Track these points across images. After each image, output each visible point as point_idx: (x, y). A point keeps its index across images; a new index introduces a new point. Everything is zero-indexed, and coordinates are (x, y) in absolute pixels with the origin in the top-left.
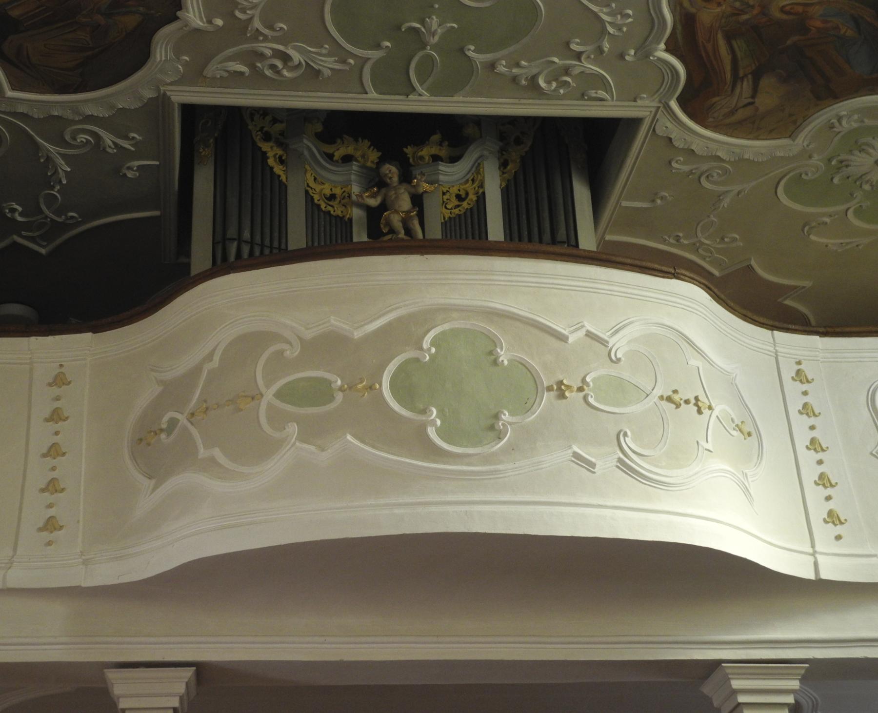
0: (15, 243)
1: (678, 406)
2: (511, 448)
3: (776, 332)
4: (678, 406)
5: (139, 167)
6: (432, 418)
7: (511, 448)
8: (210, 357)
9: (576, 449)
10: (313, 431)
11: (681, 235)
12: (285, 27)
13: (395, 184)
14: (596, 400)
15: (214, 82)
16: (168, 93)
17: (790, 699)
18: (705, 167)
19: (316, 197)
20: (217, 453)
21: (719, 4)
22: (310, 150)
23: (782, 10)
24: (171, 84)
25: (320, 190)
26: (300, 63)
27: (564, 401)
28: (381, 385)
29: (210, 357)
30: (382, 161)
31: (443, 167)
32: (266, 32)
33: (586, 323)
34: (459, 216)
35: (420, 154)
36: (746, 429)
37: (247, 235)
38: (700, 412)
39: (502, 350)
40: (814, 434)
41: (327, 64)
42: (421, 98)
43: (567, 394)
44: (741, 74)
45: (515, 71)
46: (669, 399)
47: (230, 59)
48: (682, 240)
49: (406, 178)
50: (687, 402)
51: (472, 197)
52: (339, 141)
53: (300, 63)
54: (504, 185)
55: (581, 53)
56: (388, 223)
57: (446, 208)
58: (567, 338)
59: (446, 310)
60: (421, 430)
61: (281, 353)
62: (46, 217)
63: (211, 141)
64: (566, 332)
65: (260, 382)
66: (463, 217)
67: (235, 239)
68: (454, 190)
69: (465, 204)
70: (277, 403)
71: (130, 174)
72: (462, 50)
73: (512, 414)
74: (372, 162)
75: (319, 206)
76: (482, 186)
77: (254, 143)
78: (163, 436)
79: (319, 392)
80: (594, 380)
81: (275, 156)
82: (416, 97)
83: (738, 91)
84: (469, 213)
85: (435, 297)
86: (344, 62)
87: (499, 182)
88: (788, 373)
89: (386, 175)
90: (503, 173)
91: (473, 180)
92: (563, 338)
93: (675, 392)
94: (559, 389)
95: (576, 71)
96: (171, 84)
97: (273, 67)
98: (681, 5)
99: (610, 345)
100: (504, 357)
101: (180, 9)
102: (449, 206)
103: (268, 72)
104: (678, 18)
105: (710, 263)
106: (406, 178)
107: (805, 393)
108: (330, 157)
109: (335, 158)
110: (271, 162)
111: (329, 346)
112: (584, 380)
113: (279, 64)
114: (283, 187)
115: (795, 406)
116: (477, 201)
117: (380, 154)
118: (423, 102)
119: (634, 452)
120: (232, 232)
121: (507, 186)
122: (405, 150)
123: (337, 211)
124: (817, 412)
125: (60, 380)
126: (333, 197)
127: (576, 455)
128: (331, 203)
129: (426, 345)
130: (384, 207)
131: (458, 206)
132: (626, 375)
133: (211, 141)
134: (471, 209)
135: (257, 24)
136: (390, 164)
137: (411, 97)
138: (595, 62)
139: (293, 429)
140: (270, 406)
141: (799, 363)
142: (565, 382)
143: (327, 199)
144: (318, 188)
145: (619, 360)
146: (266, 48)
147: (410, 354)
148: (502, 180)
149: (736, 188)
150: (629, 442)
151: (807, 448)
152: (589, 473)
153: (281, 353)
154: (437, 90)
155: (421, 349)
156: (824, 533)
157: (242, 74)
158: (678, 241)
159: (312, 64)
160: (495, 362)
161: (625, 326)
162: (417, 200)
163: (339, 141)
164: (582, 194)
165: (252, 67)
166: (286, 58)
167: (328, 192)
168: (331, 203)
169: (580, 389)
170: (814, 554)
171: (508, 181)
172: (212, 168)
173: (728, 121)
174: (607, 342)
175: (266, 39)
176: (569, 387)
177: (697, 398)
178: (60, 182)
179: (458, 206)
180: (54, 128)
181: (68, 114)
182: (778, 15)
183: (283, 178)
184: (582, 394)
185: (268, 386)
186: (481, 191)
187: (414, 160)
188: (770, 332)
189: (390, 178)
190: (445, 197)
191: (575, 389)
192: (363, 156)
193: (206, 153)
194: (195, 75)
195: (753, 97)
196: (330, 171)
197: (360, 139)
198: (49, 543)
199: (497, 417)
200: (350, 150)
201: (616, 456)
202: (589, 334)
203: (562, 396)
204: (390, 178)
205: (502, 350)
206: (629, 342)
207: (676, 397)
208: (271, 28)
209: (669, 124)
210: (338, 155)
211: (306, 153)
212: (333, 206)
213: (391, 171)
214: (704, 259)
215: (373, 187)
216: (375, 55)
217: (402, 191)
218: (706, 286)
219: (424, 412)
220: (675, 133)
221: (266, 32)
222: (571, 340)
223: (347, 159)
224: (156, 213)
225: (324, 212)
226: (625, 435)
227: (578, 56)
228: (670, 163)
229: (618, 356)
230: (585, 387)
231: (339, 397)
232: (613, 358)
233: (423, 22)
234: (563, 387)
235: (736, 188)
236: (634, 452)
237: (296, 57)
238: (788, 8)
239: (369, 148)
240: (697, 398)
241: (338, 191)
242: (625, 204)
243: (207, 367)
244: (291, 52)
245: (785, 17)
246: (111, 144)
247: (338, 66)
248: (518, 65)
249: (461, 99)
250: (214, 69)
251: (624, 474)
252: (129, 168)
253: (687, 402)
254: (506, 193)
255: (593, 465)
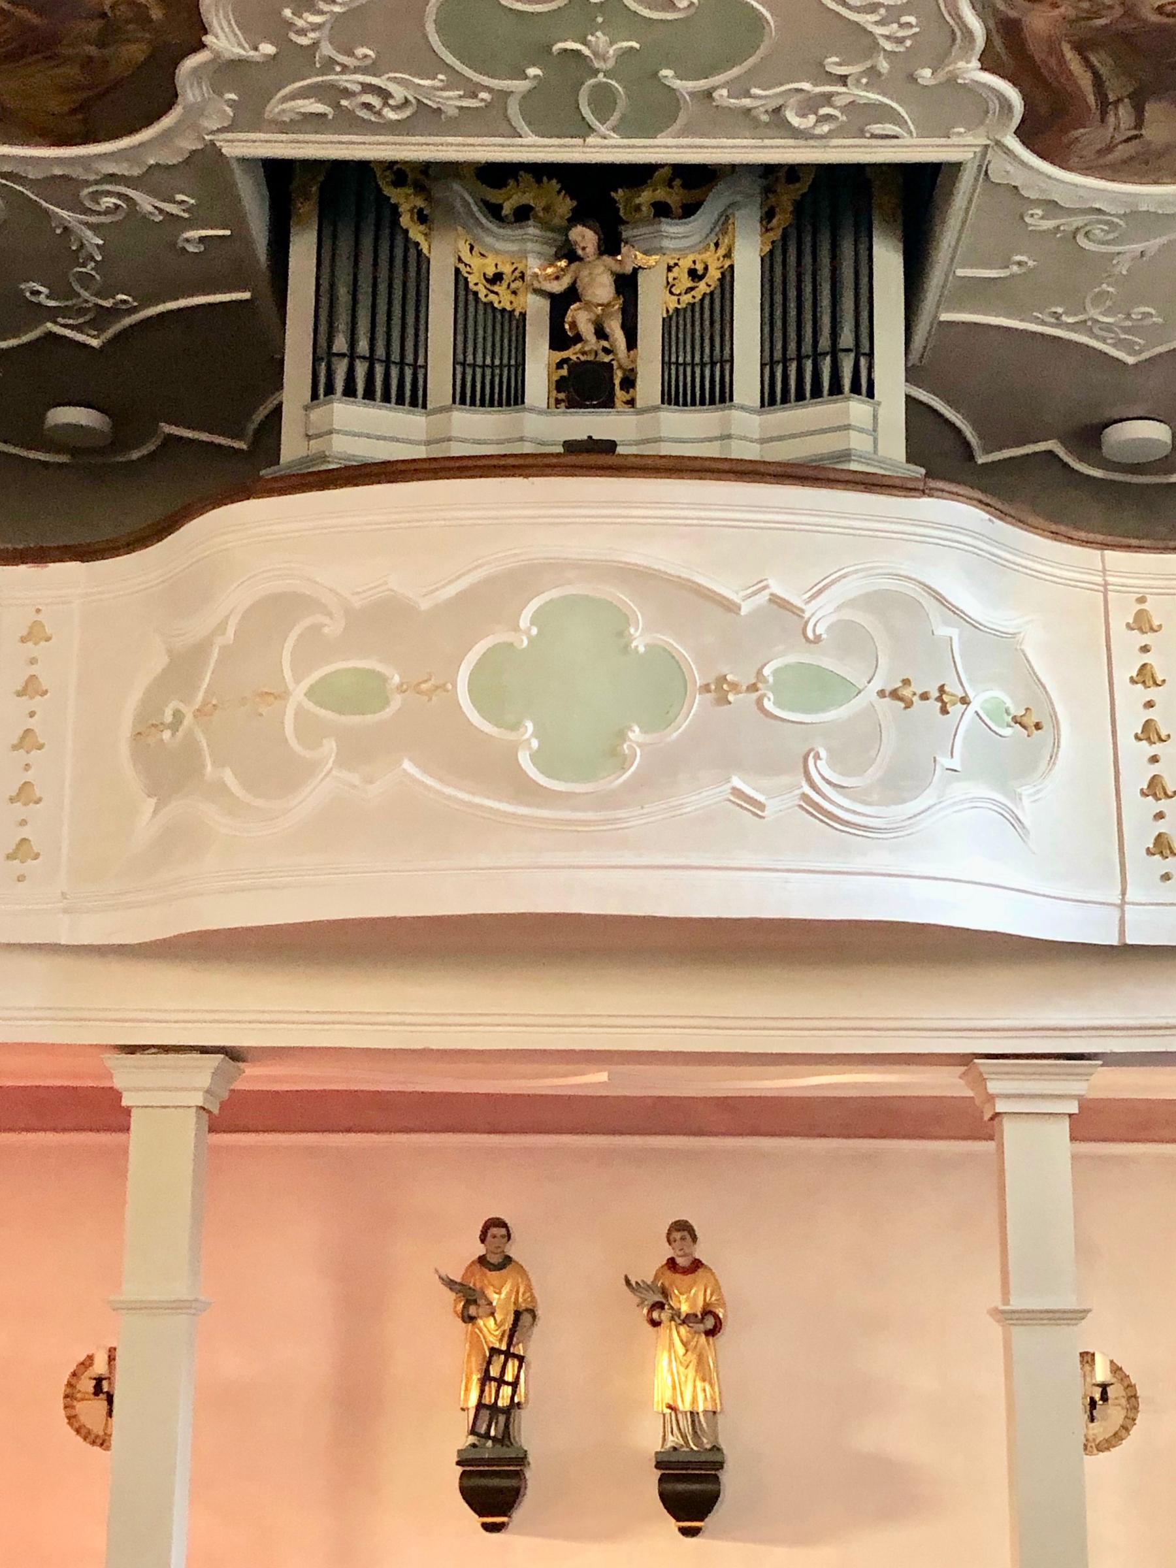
0: (50, 335)
1: (909, 705)
2: (636, 787)
3: (1109, 553)
4: (909, 705)
5: (202, 239)
6: (527, 736)
7: (640, 787)
8: (221, 627)
9: (736, 782)
10: (358, 752)
11: (1060, 310)
12: (370, 53)
13: (591, 258)
14: (777, 703)
15: (284, 127)
16: (218, 144)
17: (1074, 1108)
18: (1078, 221)
19: (472, 280)
20: (228, 776)
21: (1055, 6)
22: (463, 199)
23: (1160, 10)
24: (219, 130)
25: (479, 267)
26: (407, 101)
27: (727, 707)
28: (455, 686)
29: (221, 627)
30: (576, 218)
31: (670, 228)
32: (341, 58)
33: (771, 582)
34: (693, 305)
35: (637, 201)
36: (1031, 721)
37: (363, 346)
38: (944, 711)
39: (637, 629)
40: (1151, 714)
41: (451, 100)
42: (606, 142)
43: (731, 697)
44: (1112, 98)
45: (747, 102)
46: (895, 694)
47: (293, 97)
48: (1064, 318)
49: (610, 245)
50: (924, 697)
51: (714, 274)
52: (511, 182)
53: (407, 101)
54: (767, 249)
55: (846, 76)
56: (573, 325)
57: (671, 293)
58: (740, 608)
59: (557, 568)
60: (512, 751)
61: (316, 628)
62: (87, 301)
63: (314, 189)
64: (736, 598)
65: (288, 674)
66: (697, 309)
67: (344, 355)
68: (686, 263)
69: (702, 288)
70: (309, 705)
71: (191, 248)
72: (655, 74)
73: (644, 731)
74: (562, 217)
75: (476, 294)
76: (728, 255)
77: (380, 190)
78: (167, 735)
79: (365, 693)
80: (776, 672)
81: (411, 211)
82: (599, 141)
83: (1111, 119)
84: (707, 302)
85: (545, 545)
86: (474, 96)
87: (758, 246)
88: (1121, 617)
89: (576, 243)
90: (767, 230)
91: (717, 245)
92: (731, 607)
93: (906, 682)
94: (719, 687)
95: (840, 101)
96: (219, 130)
97: (367, 106)
98: (996, 11)
99: (807, 615)
100: (639, 642)
101: (206, 32)
102: (676, 290)
103: (364, 114)
104: (992, 25)
105: (1114, 345)
106: (610, 245)
107: (1145, 649)
108: (494, 211)
109: (504, 212)
110: (405, 221)
111: (384, 619)
112: (759, 672)
113: (375, 101)
114: (423, 262)
115: (1126, 669)
116: (722, 280)
117: (575, 203)
118: (606, 147)
119: (829, 782)
120: (341, 344)
121: (771, 252)
122: (613, 194)
123: (502, 299)
124: (1159, 679)
125: (34, 634)
126: (498, 278)
127: (736, 792)
128: (495, 288)
129: (524, 621)
130: (572, 295)
131: (692, 289)
132: (828, 663)
133: (314, 189)
134: (712, 293)
135: (327, 49)
136: (584, 225)
137: (590, 140)
138: (868, 87)
139: (330, 746)
140: (300, 712)
141: (1142, 600)
142: (728, 677)
143: (487, 280)
144: (475, 262)
145: (818, 639)
146: (351, 81)
147: (501, 636)
148: (763, 243)
149: (1138, 247)
150: (822, 768)
151: (1137, 738)
152: (757, 819)
153: (316, 628)
154: (627, 128)
155: (516, 629)
156: (1145, 869)
157: (324, 115)
158: (1057, 319)
159: (425, 101)
160: (626, 649)
161: (833, 582)
162: (627, 285)
163: (511, 182)
164: (888, 262)
165: (337, 106)
166: (385, 95)
167: (491, 271)
168: (495, 288)
169: (753, 688)
170: (1121, 907)
171: (773, 242)
172: (315, 233)
173: (1101, 161)
174: (803, 611)
175: (345, 69)
176: (734, 687)
177: (942, 689)
178: (93, 259)
179: (692, 289)
180: (63, 187)
181: (77, 172)
182: (1155, 18)
183: (424, 247)
184: (755, 696)
185: (298, 682)
186: (727, 264)
187: (625, 213)
188: (1099, 552)
189: (584, 249)
190: (671, 275)
191: (744, 688)
192: (546, 209)
193: (307, 209)
194: (249, 116)
195: (1139, 125)
196: (495, 235)
197: (545, 179)
198: (21, 879)
199: (622, 735)
200: (527, 199)
201: (798, 792)
202: (775, 600)
203: (723, 700)
204: (584, 249)
205: (637, 629)
206: (839, 608)
207: (906, 692)
208: (351, 54)
209: (1009, 168)
210: (507, 210)
211: (458, 204)
212: (497, 293)
213: (585, 237)
214: (1104, 340)
215: (559, 259)
216: (520, 86)
217: (602, 269)
218: (980, 501)
219: (515, 727)
220: (1018, 178)
221: (341, 58)
222: (743, 613)
223: (523, 214)
224: (246, 295)
225: (485, 304)
226: (817, 757)
227: (843, 80)
228: (1022, 217)
229: (818, 633)
230: (760, 685)
231: (397, 701)
232: (810, 635)
233: (585, 43)
234: (725, 687)
235: (1138, 247)
236: (829, 782)
237: (399, 93)
238: (1169, 8)
239: (559, 192)
240: (942, 689)
241: (507, 269)
242: (960, 272)
243: (219, 641)
244: (392, 87)
245: (1165, 20)
246: (150, 209)
247: (465, 103)
248: (747, 94)
249: (671, 141)
250: (275, 108)
251: (807, 816)
252: (187, 240)
253: (924, 697)
254: (768, 262)
255: (762, 807)
